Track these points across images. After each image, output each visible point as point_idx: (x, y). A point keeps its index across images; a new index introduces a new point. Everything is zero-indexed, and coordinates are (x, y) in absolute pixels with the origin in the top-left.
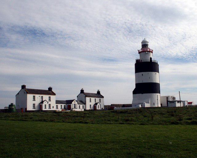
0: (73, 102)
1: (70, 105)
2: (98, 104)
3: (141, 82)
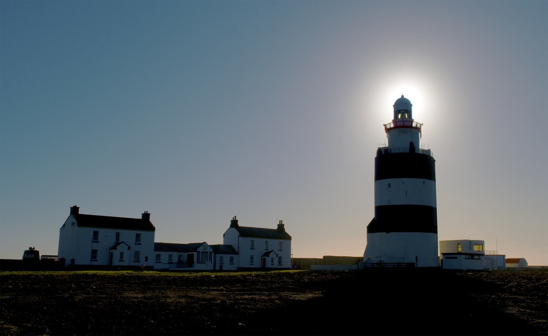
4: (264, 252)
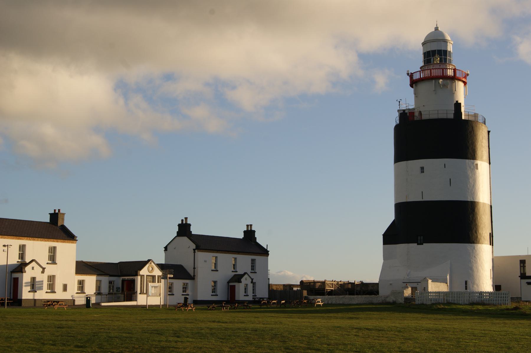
0: (146, 268)
1: (134, 280)
2: (243, 280)
3: (415, 197)
4: (230, 274)
